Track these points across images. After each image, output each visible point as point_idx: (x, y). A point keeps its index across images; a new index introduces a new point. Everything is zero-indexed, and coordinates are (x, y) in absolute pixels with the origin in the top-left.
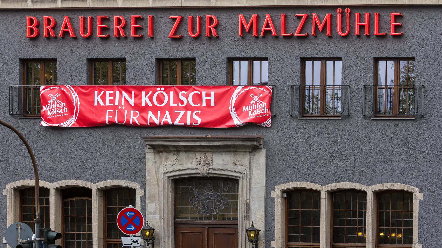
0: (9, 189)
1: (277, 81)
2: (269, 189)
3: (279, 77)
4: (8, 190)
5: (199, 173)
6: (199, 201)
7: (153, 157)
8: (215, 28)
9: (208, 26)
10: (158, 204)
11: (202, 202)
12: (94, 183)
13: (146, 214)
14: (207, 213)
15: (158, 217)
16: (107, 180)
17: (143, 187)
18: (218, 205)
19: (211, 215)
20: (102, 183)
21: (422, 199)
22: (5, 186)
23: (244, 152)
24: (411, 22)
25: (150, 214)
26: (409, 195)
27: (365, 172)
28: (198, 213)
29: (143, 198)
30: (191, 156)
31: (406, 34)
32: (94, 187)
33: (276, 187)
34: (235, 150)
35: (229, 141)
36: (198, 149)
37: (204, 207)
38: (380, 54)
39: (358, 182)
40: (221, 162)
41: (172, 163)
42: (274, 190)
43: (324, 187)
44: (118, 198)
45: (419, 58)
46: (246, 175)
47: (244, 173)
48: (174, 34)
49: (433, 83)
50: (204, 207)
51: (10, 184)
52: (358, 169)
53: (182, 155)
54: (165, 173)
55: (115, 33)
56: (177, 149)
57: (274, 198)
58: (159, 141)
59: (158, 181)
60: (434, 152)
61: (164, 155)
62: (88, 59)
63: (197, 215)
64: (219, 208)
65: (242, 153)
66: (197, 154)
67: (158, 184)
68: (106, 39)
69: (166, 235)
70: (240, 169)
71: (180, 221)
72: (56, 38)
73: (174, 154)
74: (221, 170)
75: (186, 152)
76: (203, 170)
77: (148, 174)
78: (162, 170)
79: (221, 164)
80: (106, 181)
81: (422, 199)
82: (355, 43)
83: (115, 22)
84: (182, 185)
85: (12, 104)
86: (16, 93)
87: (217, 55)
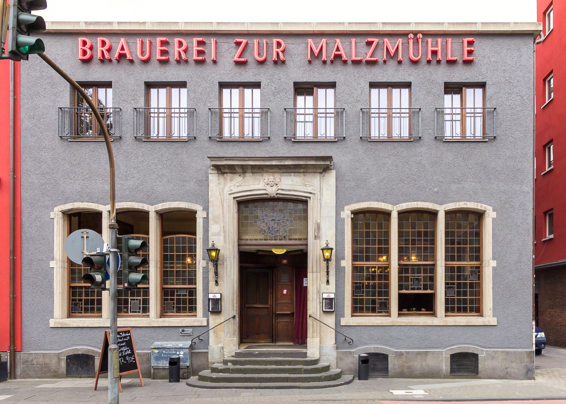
0: (57, 212)
1: (346, 105)
2: (339, 209)
3: (348, 101)
4: (489, 317)
5: (267, 194)
6: (264, 222)
7: (217, 178)
8: (283, 52)
9: (275, 50)
10: (222, 225)
11: (266, 224)
12: (152, 205)
13: (210, 235)
14: (272, 234)
15: (222, 238)
16: (166, 202)
17: (206, 209)
18: (283, 226)
19: (276, 236)
20: (160, 205)
21: (495, 217)
22: (53, 209)
23: (314, 172)
24: (482, 48)
25: (214, 235)
26: (479, 215)
27: (437, 192)
28: (263, 234)
29: (206, 220)
30: (258, 177)
31: (476, 60)
32: (152, 209)
33: (346, 208)
34: (305, 171)
35: (302, 160)
36: (266, 170)
37: (269, 228)
38: (451, 79)
39: (431, 202)
40: (290, 183)
41: (237, 184)
42: (343, 210)
43: (395, 207)
44: (179, 224)
45: (490, 83)
46: (316, 195)
47: (314, 194)
48: (240, 57)
49: (504, 106)
50: (269, 228)
51: (58, 207)
52: (430, 189)
53: (249, 176)
54: (230, 194)
55: (176, 56)
56: (244, 170)
57: (344, 219)
58: (226, 160)
59: (222, 202)
60: (507, 172)
61: (229, 176)
62: (145, 82)
63: (262, 237)
64: (285, 229)
65: (311, 174)
66: (264, 174)
67: (223, 206)
68: (164, 62)
69: (232, 256)
70: (309, 189)
71: (243, 242)
72: (110, 61)
73: (240, 176)
74: (290, 190)
75: (253, 173)
76: (272, 191)
77: (211, 196)
78: (227, 191)
79: (290, 184)
80: (164, 204)
81: (495, 217)
82: (425, 69)
83: (176, 45)
84: (245, 204)
85: (62, 127)
86: (67, 116)
87: (284, 80)
